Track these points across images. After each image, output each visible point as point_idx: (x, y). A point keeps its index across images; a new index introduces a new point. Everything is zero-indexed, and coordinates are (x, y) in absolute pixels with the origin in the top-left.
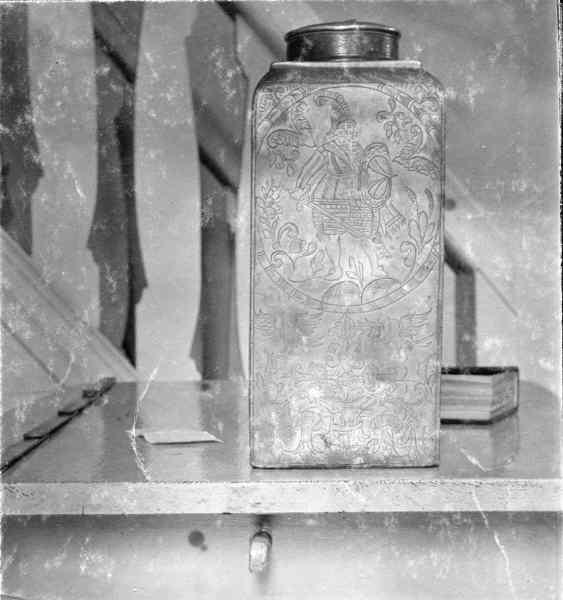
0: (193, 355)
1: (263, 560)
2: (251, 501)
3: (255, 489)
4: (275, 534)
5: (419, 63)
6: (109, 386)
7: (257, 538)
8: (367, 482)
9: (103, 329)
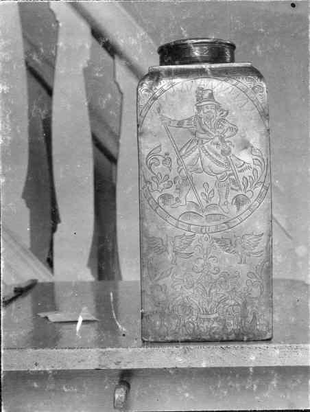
0: (89, 265)
1: (123, 401)
2: (115, 361)
3: (117, 352)
4: (132, 385)
6: (33, 285)
8: (192, 348)
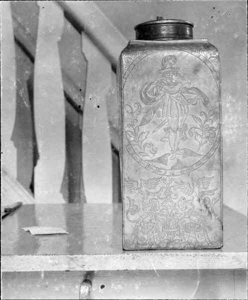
1: (86, 295)
5: (207, 40)
7: (84, 283)
9: (19, 179)
